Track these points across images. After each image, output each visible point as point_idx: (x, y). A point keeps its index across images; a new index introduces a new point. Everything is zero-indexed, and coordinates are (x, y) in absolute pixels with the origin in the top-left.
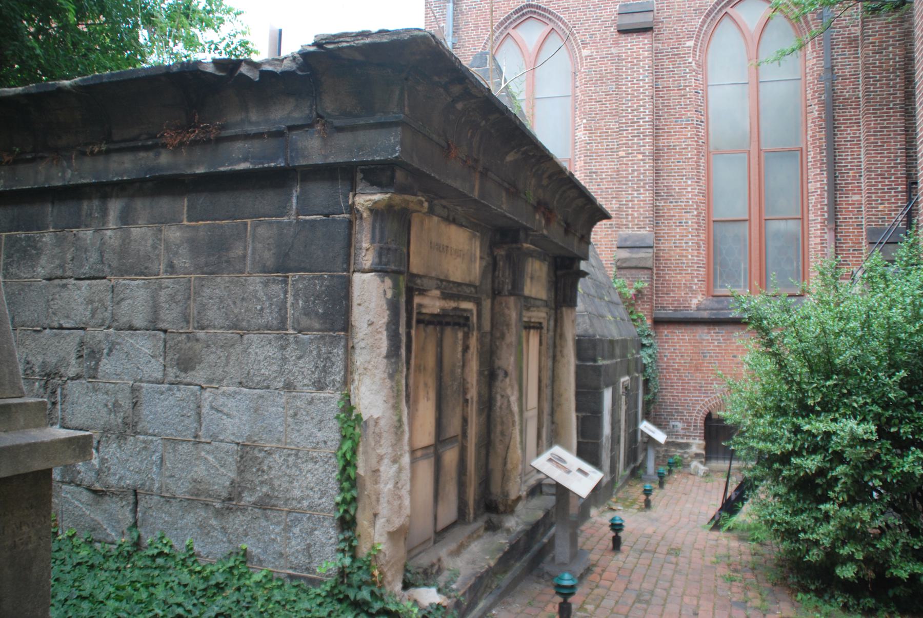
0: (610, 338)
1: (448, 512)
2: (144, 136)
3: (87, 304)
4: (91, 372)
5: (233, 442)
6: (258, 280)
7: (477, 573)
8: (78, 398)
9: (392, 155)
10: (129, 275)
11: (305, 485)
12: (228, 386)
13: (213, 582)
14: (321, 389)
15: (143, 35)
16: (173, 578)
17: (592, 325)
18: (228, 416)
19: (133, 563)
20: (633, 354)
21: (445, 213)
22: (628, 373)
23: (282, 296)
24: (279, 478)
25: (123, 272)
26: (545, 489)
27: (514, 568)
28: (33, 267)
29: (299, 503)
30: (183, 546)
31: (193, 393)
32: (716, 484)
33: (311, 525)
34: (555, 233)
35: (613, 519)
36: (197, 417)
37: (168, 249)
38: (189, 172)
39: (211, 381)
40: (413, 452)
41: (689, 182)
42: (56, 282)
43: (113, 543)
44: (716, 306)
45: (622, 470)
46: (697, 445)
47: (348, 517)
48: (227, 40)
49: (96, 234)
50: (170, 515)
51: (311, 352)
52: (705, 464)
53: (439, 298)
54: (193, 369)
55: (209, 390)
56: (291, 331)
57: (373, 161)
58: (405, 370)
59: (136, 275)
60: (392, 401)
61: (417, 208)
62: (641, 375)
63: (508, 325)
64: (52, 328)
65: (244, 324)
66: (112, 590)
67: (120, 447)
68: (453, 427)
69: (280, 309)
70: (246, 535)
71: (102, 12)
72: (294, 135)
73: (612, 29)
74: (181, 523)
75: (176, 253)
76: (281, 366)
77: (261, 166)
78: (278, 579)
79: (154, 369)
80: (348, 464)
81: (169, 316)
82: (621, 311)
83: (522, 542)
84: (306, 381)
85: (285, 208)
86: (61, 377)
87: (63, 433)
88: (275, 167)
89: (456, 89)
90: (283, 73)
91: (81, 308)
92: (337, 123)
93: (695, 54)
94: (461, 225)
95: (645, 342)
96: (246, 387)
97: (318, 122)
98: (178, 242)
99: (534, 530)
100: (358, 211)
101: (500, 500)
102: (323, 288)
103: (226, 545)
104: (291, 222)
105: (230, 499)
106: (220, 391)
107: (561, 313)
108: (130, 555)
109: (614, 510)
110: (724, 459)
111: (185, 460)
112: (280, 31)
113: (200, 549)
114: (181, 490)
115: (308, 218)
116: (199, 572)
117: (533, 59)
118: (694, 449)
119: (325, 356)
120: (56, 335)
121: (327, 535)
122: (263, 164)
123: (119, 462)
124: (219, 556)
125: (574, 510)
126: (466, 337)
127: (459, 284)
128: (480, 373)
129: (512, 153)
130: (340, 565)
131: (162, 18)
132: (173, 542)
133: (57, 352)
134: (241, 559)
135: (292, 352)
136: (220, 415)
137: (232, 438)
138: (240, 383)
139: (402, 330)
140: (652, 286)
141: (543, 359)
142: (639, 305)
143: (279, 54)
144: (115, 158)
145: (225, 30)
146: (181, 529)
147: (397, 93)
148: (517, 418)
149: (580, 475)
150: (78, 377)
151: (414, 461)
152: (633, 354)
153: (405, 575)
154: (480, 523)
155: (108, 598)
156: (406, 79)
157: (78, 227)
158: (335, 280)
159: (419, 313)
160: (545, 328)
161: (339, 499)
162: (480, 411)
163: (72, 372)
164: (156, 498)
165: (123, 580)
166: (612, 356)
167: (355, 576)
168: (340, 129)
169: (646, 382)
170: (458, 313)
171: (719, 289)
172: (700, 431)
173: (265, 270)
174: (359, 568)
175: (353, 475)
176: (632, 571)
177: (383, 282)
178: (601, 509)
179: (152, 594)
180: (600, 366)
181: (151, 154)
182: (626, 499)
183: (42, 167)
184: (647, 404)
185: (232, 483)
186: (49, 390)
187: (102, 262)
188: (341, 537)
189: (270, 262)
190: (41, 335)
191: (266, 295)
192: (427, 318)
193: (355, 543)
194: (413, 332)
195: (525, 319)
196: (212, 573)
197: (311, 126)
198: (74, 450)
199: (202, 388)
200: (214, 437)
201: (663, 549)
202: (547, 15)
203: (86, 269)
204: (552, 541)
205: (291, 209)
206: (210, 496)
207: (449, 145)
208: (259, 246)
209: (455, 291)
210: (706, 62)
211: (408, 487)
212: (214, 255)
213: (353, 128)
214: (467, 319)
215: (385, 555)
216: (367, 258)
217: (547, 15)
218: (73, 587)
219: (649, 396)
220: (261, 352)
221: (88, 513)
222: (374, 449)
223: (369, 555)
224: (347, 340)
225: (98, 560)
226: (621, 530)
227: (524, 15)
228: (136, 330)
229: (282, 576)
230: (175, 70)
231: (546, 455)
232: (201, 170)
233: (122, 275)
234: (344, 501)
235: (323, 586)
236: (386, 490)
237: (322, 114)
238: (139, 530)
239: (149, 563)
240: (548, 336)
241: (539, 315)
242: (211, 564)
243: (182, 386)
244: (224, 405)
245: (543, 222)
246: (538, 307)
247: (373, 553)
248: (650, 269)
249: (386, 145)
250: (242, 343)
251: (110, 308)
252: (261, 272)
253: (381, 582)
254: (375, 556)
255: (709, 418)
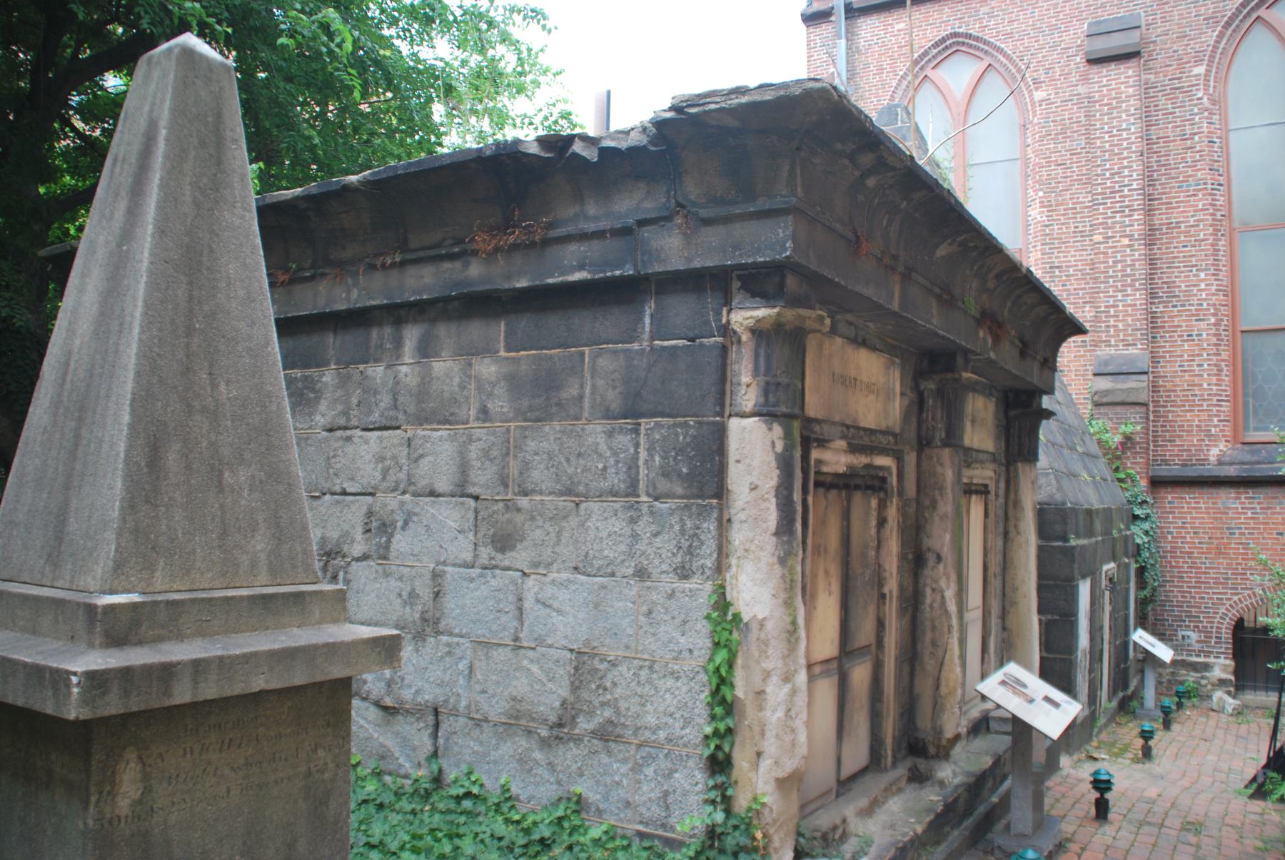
0: (1086, 506)
1: (856, 755)
2: (449, 242)
3: (377, 462)
4: (382, 551)
5: (565, 648)
6: (599, 428)
7: (898, 842)
8: (365, 584)
9: (780, 254)
10: (431, 423)
11: (661, 709)
12: (558, 572)
13: (536, 837)
14: (685, 577)
15: (438, 111)
16: (483, 828)
17: (1060, 488)
18: (559, 611)
19: (432, 804)
20: (1120, 531)
21: (851, 332)
22: (1114, 559)
23: (632, 450)
24: (626, 698)
25: (422, 419)
26: (993, 725)
27: (950, 838)
28: (310, 414)
29: (654, 733)
30: (497, 786)
31: (514, 582)
32: (1254, 727)
33: (669, 765)
34: (1006, 356)
35: (1096, 773)
36: (517, 613)
37: (480, 388)
38: (507, 286)
39: (536, 565)
40: (810, 666)
41: (1202, 275)
42: (339, 433)
43: (406, 777)
44: (1248, 458)
45: (1106, 702)
46: (1222, 667)
47: (720, 755)
48: (545, 112)
49: (389, 371)
50: (481, 743)
51: (672, 526)
52: (1234, 698)
53: (845, 452)
54: (513, 548)
55: (533, 577)
56: (644, 498)
57: (755, 263)
58: (801, 552)
59: (439, 423)
60: (783, 595)
61: (816, 326)
62: (1132, 561)
63: (942, 489)
64: (333, 494)
65: (581, 488)
66: (407, 838)
67: (417, 650)
68: (865, 633)
69: (630, 468)
70: (581, 775)
71: (388, 89)
72: (646, 232)
73: (1078, 59)
74: (494, 755)
75: (491, 395)
76: (631, 546)
77: (601, 275)
78: (624, 837)
79: (462, 548)
80: (722, 682)
81: (482, 477)
82: (1102, 467)
83: (961, 800)
84: (665, 567)
85: (635, 330)
86: (344, 557)
87: (366, 632)
88: (621, 276)
89: (867, 159)
90: (630, 149)
91: (370, 467)
92: (704, 213)
93: (1206, 86)
94: (873, 349)
95: (1138, 512)
96: (583, 574)
97: (678, 213)
98: (493, 379)
99: (978, 785)
100: (735, 332)
101: (929, 738)
102: (688, 440)
103: (555, 787)
104: (643, 350)
105: (560, 725)
106: (548, 579)
107: (1016, 471)
108: (427, 795)
109: (1096, 759)
110: (1267, 689)
111: (501, 671)
112: (609, 93)
113: (520, 792)
114: (496, 709)
115: (666, 343)
116: (518, 822)
117: (962, 109)
118: (1217, 673)
119: (691, 532)
120: (338, 502)
121: (692, 780)
122: (604, 272)
123: (420, 674)
124: (544, 802)
125: (1039, 755)
126: (882, 506)
127: (872, 432)
128: (902, 557)
129: (945, 245)
130: (709, 821)
131: (462, 88)
132: (484, 780)
133: (339, 525)
134: (573, 807)
135: (645, 527)
136: (548, 611)
137: (564, 642)
138: (576, 568)
139: (797, 497)
140: (1148, 429)
141: (990, 536)
142: (1128, 458)
143: (608, 128)
144: (412, 271)
145: (543, 96)
146: (495, 762)
147: (786, 168)
148: (955, 622)
149: (1047, 706)
150: (365, 557)
151: (811, 678)
152: (1120, 531)
153: (797, 841)
154: (902, 771)
155: (402, 848)
156: (798, 149)
157: (366, 362)
158: (705, 427)
159: (818, 473)
160: (993, 492)
161: (708, 730)
162: (902, 611)
163: (357, 550)
164: (462, 720)
165: (420, 826)
166: (1090, 533)
167: (729, 838)
168: (707, 222)
169: (1141, 571)
170: (872, 472)
171: (1252, 433)
172: (1227, 646)
173: (608, 415)
174: (736, 827)
175: (729, 698)
176: (1127, 851)
177: (770, 429)
178: (1075, 757)
179: (458, 848)
180: (1073, 548)
181: (458, 265)
182: (1113, 744)
183: (322, 287)
184: (1143, 603)
185: (564, 703)
186: (329, 574)
187: (396, 407)
188: (711, 783)
189: (615, 406)
190: (319, 502)
191: (610, 448)
192: (829, 479)
193: (729, 792)
194: (810, 499)
195: (965, 480)
196: (535, 823)
197: (668, 218)
198: (379, 653)
199: (525, 574)
200: (540, 641)
201: (1174, 822)
202: (981, 46)
203: (375, 417)
204: (1005, 802)
205: (643, 332)
206: (533, 720)
207: (858, 237)
208: (600, 382)
209: (866, 441)
210: (1225, 96)
211: (804, 716)
212: (540, 396)
213: (726, 220)
214: (884, 480)
215: (771, 810)
216: (748, 397)
217: (981, 46)
218: (358, 830)
219: (1146, 593)
220: (604, 526)
221: (376, 735)
222: (758, 662)
223: (749, 809)
224: (721, 511)
225: (387, 798)
226: (1109, 789)
227: (947, 48)
228: (438, 496)
229: (629, 833)
230: (488, 153)
231: (998, 676)
232: (522, 283)
233: (421, 424)
234: (716, 733)
235: (684, 850)
236: (774, 719)
237: (684, 202)
238: (440, 761)
239: (452, 805)
240: (997, 504)
241: (983, 474)
242: (533, 812)
243: (498, 572)
244: (553, 597)
245: (990, 341)
246: (982, 462)
247: (754, 806)
248: (1145, 405)
249: (774, 241)
250: (577, 514)
251: (405, 467)
252: (604, 418)
253: (764, 848)
254: (758, 812)
255: (1239, 626)
